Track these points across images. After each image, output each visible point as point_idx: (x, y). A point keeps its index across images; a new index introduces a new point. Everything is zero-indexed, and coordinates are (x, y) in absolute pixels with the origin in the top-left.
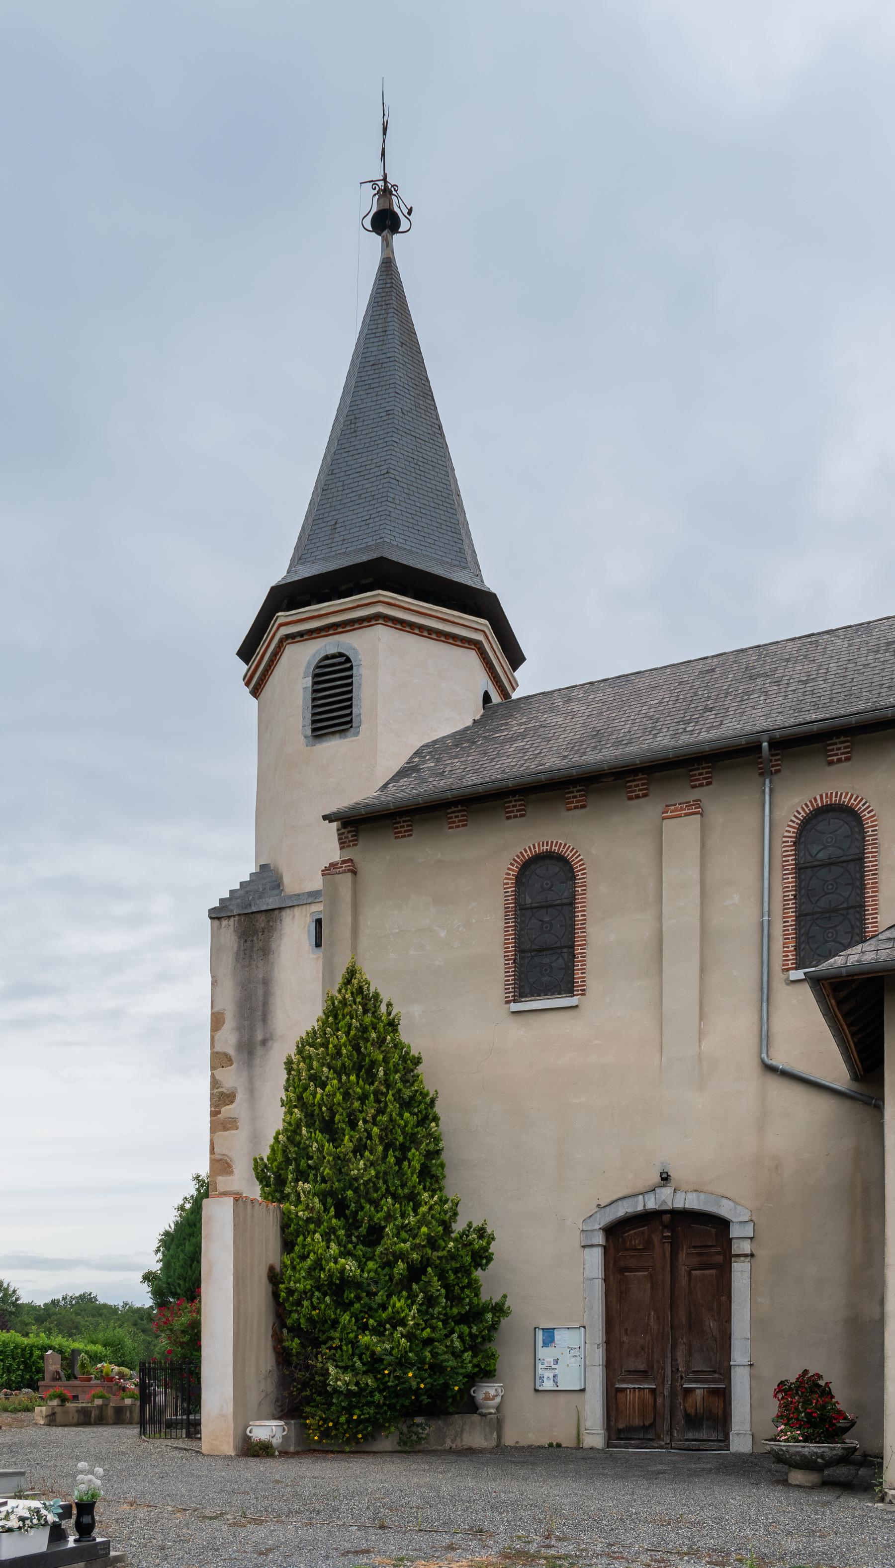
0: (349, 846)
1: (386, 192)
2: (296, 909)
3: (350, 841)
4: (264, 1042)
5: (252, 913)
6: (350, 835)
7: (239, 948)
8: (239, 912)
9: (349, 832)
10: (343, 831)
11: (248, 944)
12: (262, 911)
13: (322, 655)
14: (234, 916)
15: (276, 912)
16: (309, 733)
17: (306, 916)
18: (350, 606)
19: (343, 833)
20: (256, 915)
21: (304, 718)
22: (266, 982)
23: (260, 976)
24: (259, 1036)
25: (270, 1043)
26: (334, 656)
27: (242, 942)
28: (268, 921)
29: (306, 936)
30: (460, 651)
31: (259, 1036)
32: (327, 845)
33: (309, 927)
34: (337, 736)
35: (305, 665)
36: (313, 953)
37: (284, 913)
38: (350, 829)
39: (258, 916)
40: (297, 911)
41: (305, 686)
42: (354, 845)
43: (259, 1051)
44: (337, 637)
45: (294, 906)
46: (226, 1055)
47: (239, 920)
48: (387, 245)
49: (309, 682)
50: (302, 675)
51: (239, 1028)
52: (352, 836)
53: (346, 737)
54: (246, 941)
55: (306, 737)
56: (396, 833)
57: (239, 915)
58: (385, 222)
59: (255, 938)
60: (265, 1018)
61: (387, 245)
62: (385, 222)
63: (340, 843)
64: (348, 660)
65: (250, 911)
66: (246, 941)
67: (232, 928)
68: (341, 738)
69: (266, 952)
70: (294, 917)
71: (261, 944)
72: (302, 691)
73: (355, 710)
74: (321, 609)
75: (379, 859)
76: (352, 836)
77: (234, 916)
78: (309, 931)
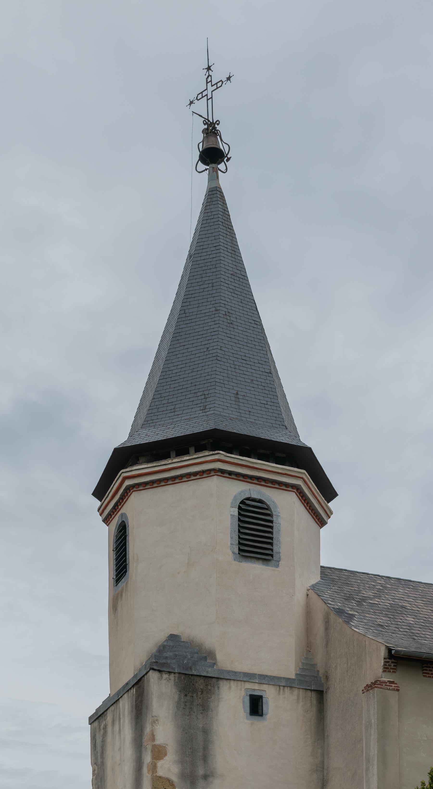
0: (390, 671)
1: (211, 130)
2: (232, 682)
3: (391, 669)
4: (205, 777)
5: (192, 675)
6: (392, 665)
7: (180, 699)
8: (179, 671)
9: (392, 662)
10: (388, 660)
11: (188, 698)
12: (200, 676)
13: (247, 496)
14: (175, 673)
15: (214, 680)
16: (237, 551)
17: (241, 690)
18: (280, 471)
19: (388, 662)
20: (196, 678)
21: (232, 538)
22: (206, 732)
23: (201, 726)
24: (201, 771)
25: (211, 779)
26: (254, 500)
27: (183, 695)
28: (207, 685)
29: (242, 705)
30: (160, 489)
31: (201, 771)
32: (374, 665)
33: (244, 698)
34: (261, 562)
35: (232, 498)
36: (247, 719)
37: (221, 683)
38: (393, 660)
39: (197, 679)
40: (232, 683)
41: (232, 513)
42: (393, 672)
43: (201, 784)
44: (259, 487)
45: (230, 679)
46: (169, 780)
47: (179, 678)
48: (214, 177)
49: (235, 511)
50: (229, 504)
51: (182, 762)
52: (394, 666)
53: (267, 565)
54: (186, 695)
55: (233, 553)
56: (423, 673)
57: (179, 673)
58: (212, 155)
59: (195, 695)
60: (205, 758)
61: (214, 177)
62: (212, 155)
63: (385, 668)
64: (268, 508)
65: (191, 673)
66: (186, 695)
67: (172, 682)
68: (263, 564)
69: (205, 708)
70: (230, 688)
71: (200, 701)
72: (229, 516)
73: (275, 548)
74: (256, 463)
75: (413, 687)
76: (394, 666)
77: (175, 673)
78: (244, 702)
